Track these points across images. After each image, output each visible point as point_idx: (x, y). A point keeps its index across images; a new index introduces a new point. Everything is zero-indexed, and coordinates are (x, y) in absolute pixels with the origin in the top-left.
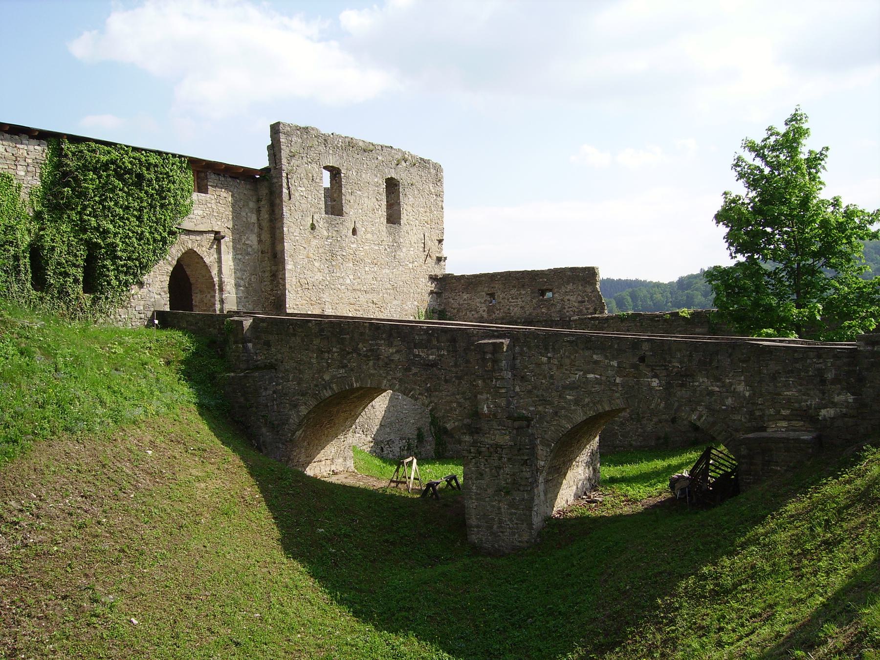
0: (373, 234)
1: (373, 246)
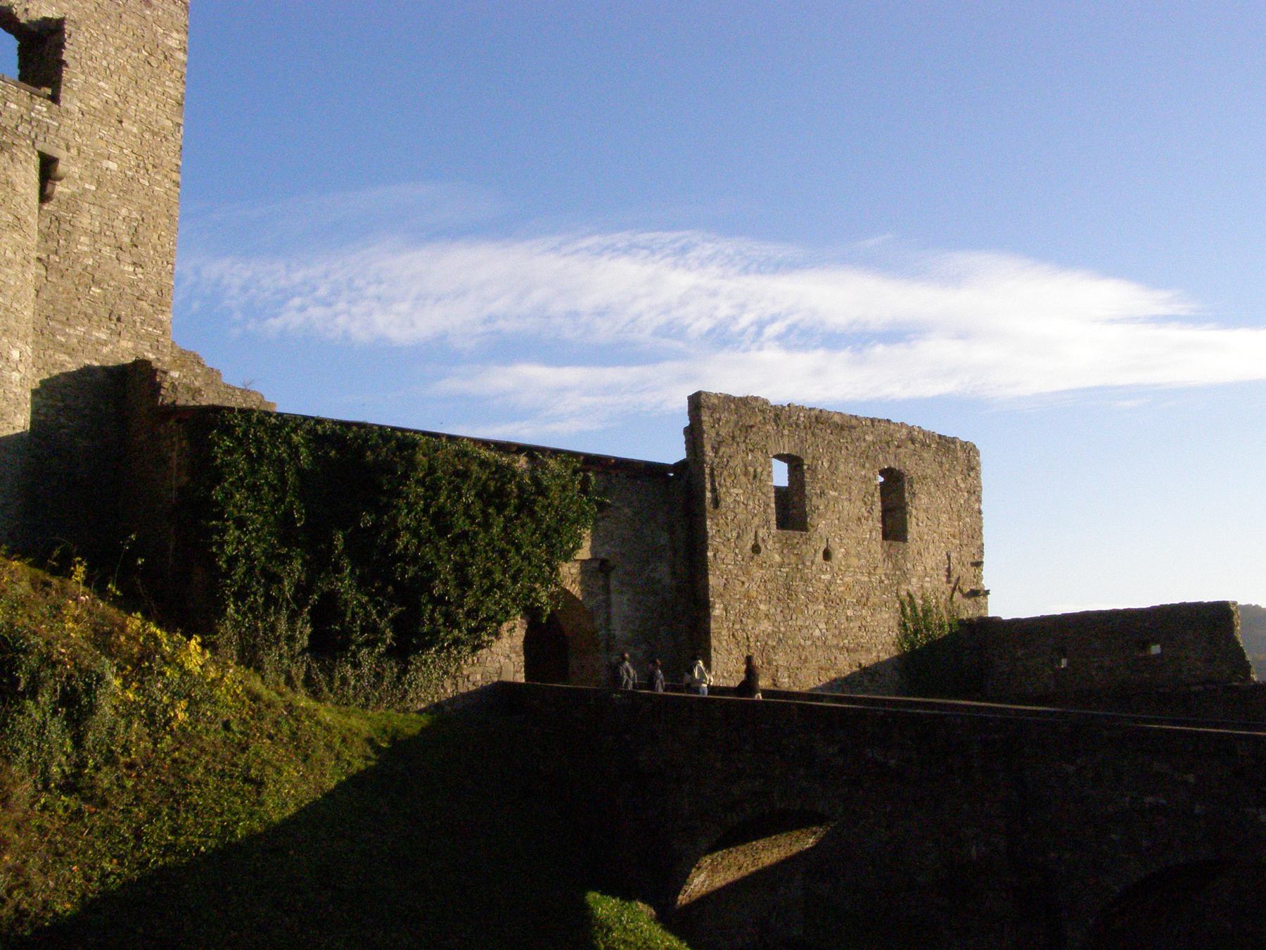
0: (858, 556)
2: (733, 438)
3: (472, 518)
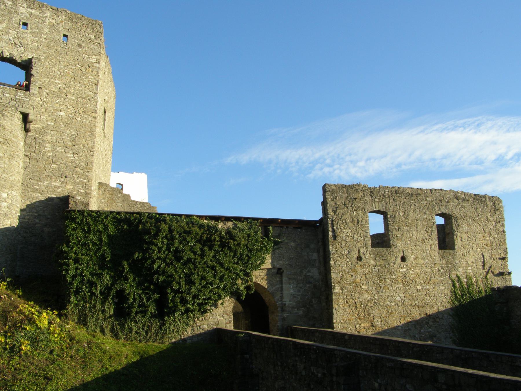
0: (424, 259)
1: (424, 269)
2: (345, 205)
3: (195, 253)
